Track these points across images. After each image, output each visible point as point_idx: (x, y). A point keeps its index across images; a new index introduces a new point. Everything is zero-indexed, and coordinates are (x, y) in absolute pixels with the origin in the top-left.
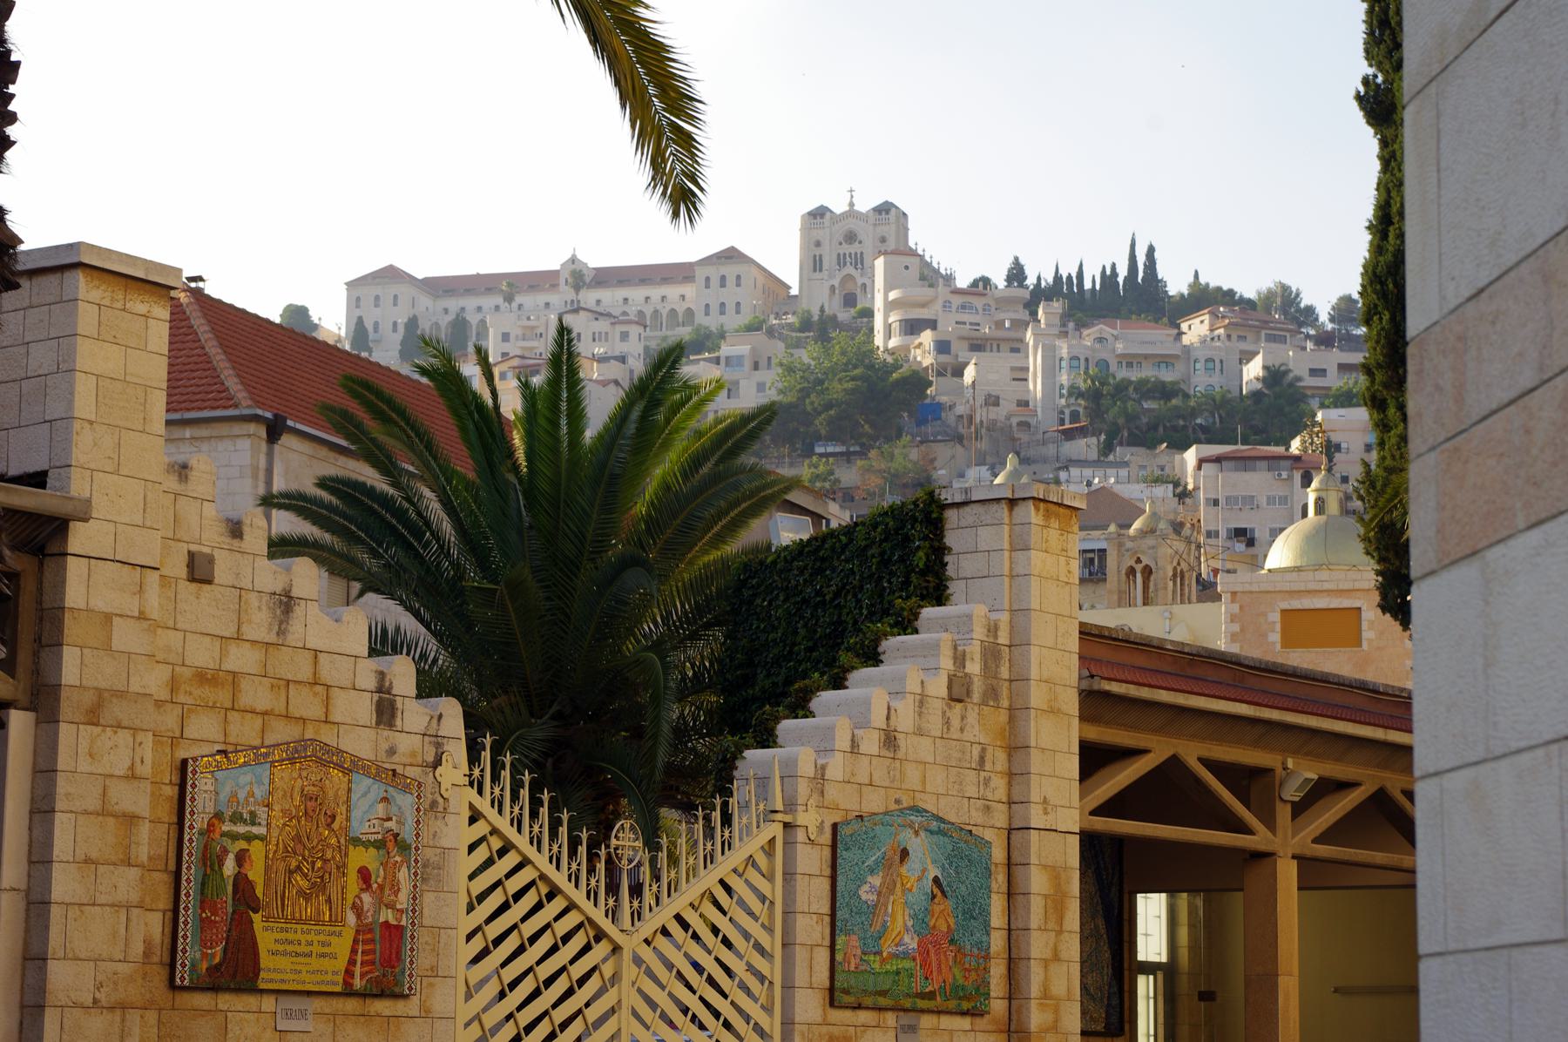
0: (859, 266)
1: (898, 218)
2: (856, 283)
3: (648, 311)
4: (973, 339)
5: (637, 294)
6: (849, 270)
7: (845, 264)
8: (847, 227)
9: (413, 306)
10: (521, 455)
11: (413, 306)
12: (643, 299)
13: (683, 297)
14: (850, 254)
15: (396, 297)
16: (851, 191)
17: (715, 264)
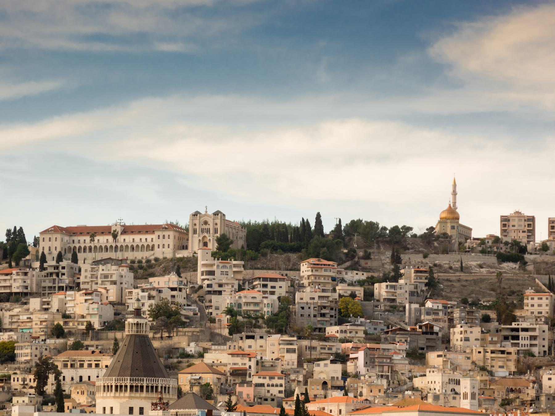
1: (221, 217)
6: (205, 234)
15: (56, 238)
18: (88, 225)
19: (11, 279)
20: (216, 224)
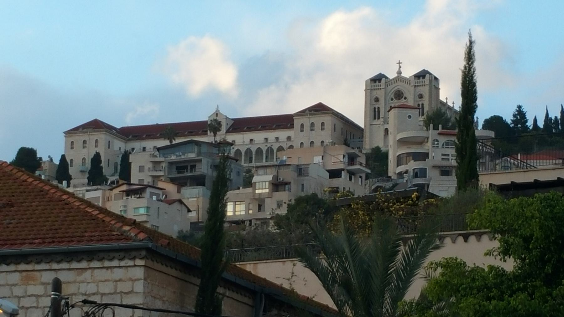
1: (430, 81)
3: (254, 149)
4: (443, 167)
5: (259, 137)
8: (397, 88)
9: (109, 148)
10: (395, 277)
11: (109, 148)
12: (249, 140)
13: (266, 139)
15: (97, 141)
16: (399, 63)
18: (159, 123)
20: (421, 96)
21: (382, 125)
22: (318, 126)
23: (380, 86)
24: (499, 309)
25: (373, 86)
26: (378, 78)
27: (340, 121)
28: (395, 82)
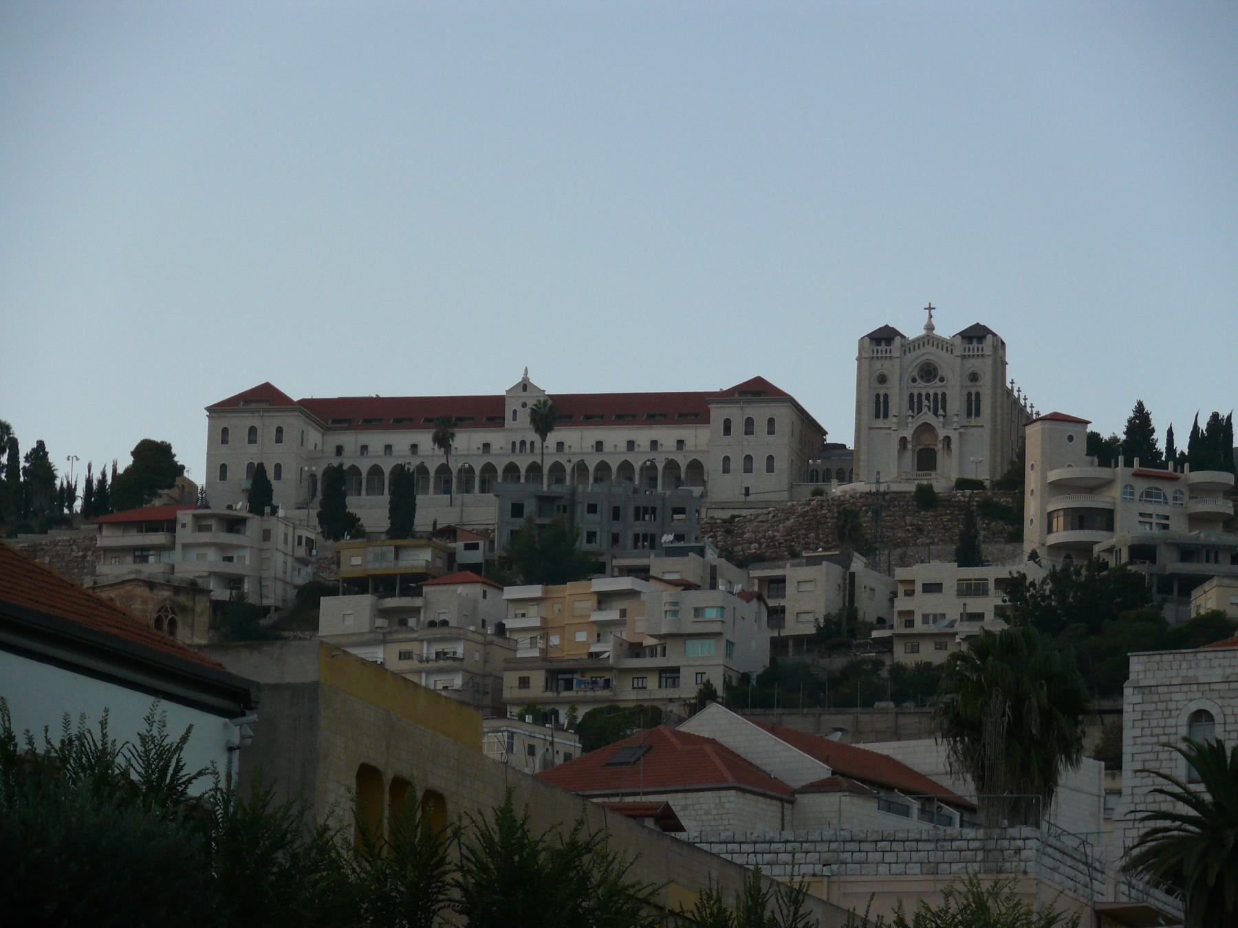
0: (941, 412)
1: (995, 348)
2: (936, 436)
5: (615, 437)
6: (927, 417)
7: (920, 410)
8: (925, 357)
9: (302, 445)
11: (302, 445)
12: (648, 444)
13: (487, 446)
14: (928, 396)
15: (279, 431)
16: (930, 308)
17: (738, 402)
19: (171, 547)
21: (894, 430)
22: (761, 426)
23: (982, 350)
24: (773, 724)
25: (967, 350)
26: (885, 336)
27: (798, 415)
28: (917, 347)
